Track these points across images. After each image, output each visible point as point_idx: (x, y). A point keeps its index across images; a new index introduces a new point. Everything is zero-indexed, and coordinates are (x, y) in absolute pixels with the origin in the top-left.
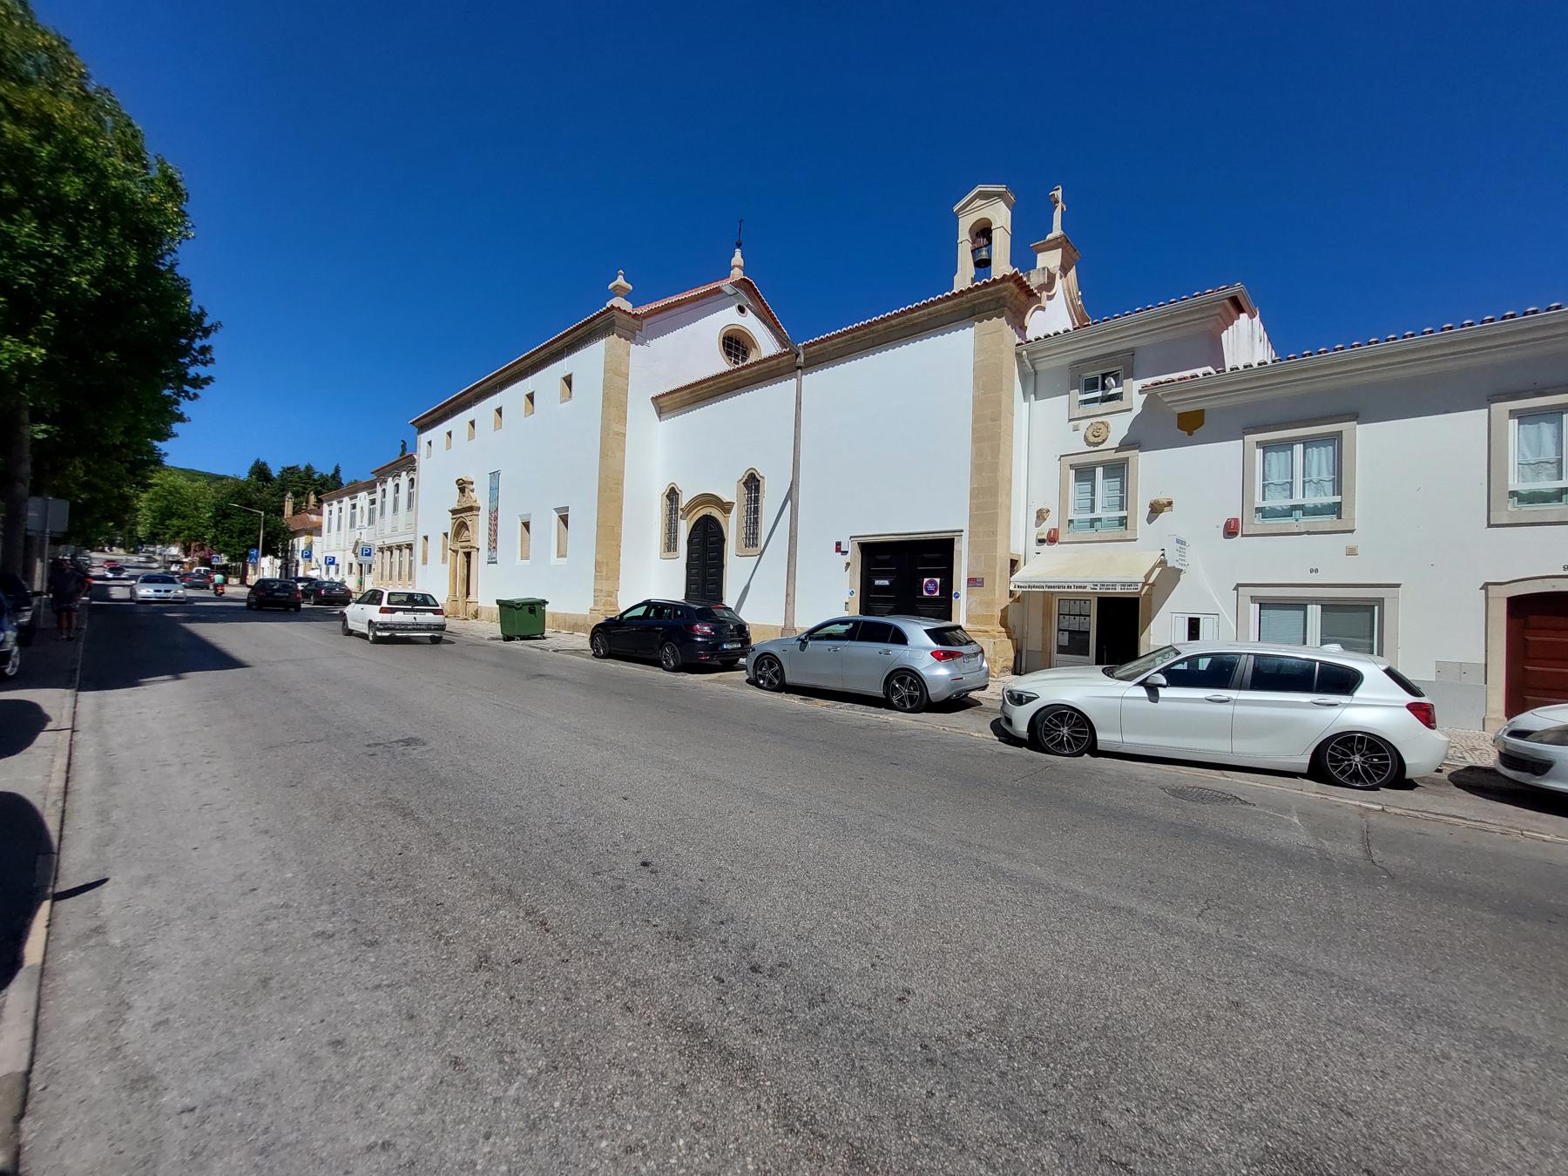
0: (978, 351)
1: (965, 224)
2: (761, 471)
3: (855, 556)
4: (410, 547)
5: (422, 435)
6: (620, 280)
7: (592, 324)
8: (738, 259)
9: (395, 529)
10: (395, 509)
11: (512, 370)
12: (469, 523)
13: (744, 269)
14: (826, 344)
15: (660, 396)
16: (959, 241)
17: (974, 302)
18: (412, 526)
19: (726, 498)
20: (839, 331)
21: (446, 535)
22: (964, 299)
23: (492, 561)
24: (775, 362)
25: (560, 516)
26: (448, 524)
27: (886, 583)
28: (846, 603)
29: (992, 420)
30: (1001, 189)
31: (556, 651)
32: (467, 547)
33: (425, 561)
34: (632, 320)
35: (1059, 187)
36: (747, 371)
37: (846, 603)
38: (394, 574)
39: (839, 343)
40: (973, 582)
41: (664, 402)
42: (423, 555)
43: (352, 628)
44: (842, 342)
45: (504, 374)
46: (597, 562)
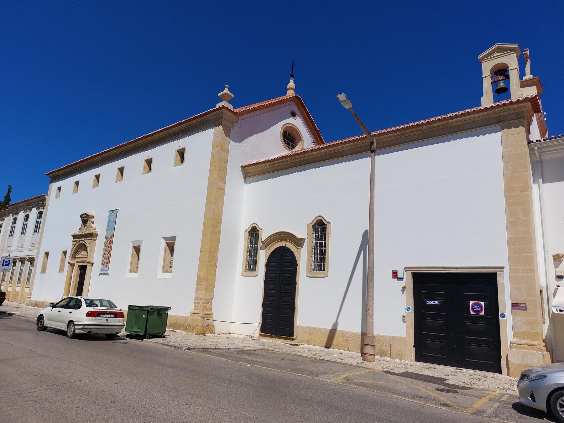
0: (504, 146)
1: (487, 67)
2: (327, 218)
3: (408, 282)
4: (32, 260)
5: (53, 184)
6: (226, 91)
7: (205, 117)
8: (291, 84)
9: (20, 246)
10: (23, 232)
11: (136, 143)
12: (88, 245)
13: (296, 90)
14: (381, 137)
15: (248, 166)
16: (483, 76)
17: (500, 114)
18: (37, 245)
19: (299, 236)
20: (145, 135)
21: (65, 253)
22: (492, 112)
23: (104, 273)
24: (339, 147)
25: (167, 243)
26: (69, 245)
27: (437, 303)
28: (404, 317)
29: (522, 191)
30: (515, 46)
31: (189, 349)
32: (84, 262)
33: (44, 270)
34: (233, 116)
35: (528, 49)
36: (318, 152)
37: (404, 317)
38: (14, 279)
39: (391, 137)
40: (515, 306)
41: (250, 169)
42: (43, 266)
43: (47, 325)
44: (393, 136)
45: (128, 146)
46: (199, 278)
